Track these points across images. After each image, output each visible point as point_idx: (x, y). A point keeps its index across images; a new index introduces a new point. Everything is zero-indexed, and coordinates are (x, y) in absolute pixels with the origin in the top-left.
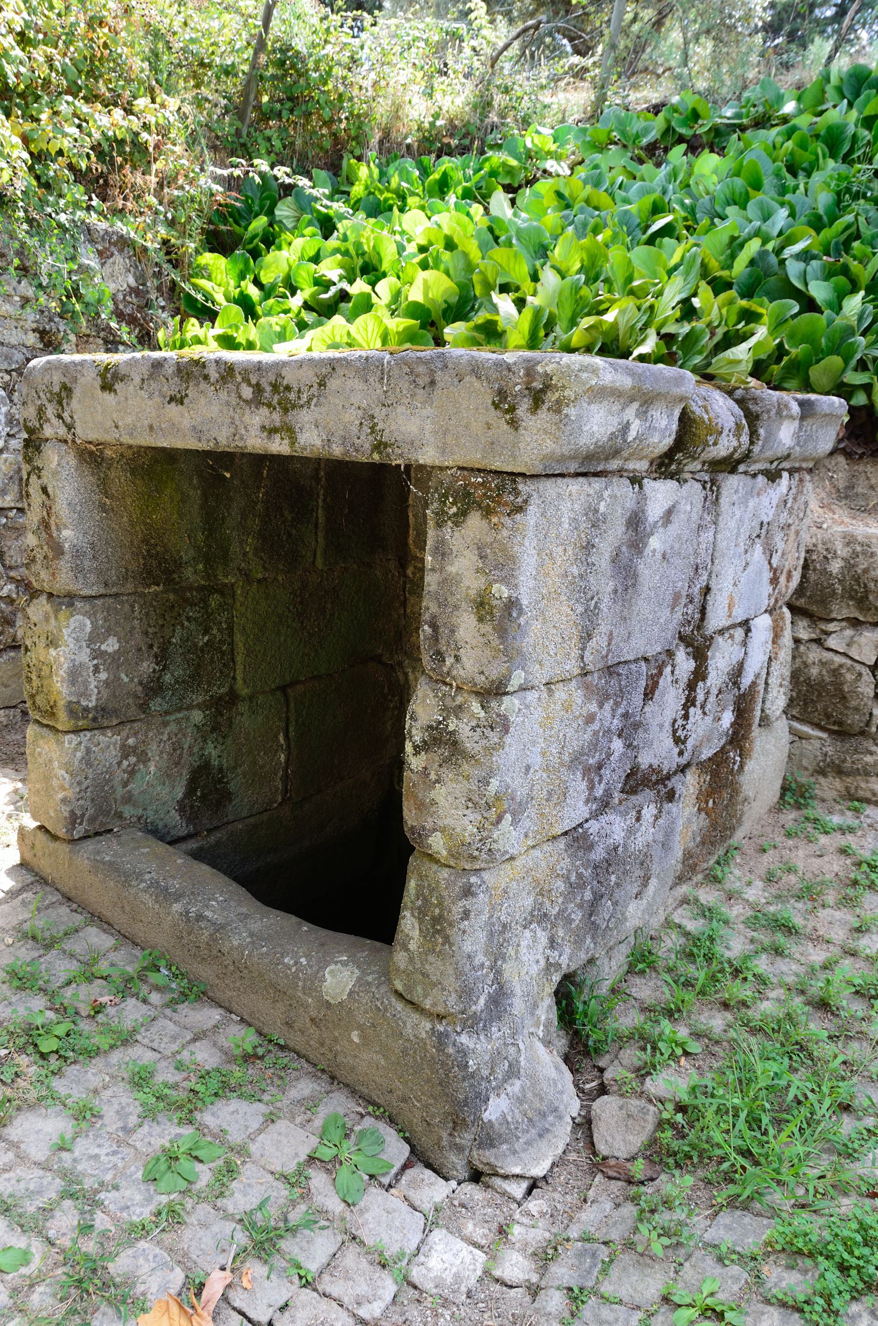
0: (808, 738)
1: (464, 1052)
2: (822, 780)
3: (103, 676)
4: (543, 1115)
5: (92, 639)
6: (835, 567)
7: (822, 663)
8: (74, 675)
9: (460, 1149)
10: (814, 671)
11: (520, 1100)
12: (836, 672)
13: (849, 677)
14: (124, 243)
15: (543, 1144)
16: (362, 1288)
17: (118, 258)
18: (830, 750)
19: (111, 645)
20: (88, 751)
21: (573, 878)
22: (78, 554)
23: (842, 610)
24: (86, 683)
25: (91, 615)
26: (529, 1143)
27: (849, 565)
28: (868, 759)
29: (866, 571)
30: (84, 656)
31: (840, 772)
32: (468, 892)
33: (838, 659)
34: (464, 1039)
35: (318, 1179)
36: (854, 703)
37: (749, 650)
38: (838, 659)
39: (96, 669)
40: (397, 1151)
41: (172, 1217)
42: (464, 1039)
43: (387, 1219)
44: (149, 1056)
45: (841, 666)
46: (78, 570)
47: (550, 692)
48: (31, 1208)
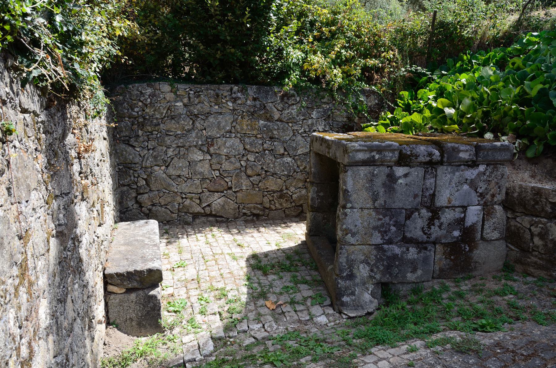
0: (512, 250)
1: (338, 283)
2: (517, 265)
3: (319, 201)
4: (358, 306)
5: (317, 192)
6: (516, 195)
7: (515, 226)
8: (312, 199)
9: (337, 305)
10: (513, 228)
11: (353, 301)
12: (518, 229)
13: (522, 231)
14: (373, 92)
15: (355, 311)
16: (303, 316)
17: (372, 97)
18: (518, 255)
19: (321, 194)
20: (315, 216)
21: (378, 257)
22: (314, 174)
23: (519, 209)
24: (315, 201)
25: (317, 187)
26: (351, 309)
27: (520, 194)
28: (529, 260)
29: (525, 197)
30: (315, 196)
31: (522, 264)
32: (341, 249)
33: (519, 225)
34: (339, 281)
35: (309, 300)
36: (523, 240)
37: (467, 215)
38: (519, 225)
39: (318, 199)
40: (328, 302)
41: (281, 294)
42: (339, 281)
43: (316, 310)
44: (299, 275)
45: (520, 227)
46: (314, 177)
47: (362, 211)
48: (263, 285)
